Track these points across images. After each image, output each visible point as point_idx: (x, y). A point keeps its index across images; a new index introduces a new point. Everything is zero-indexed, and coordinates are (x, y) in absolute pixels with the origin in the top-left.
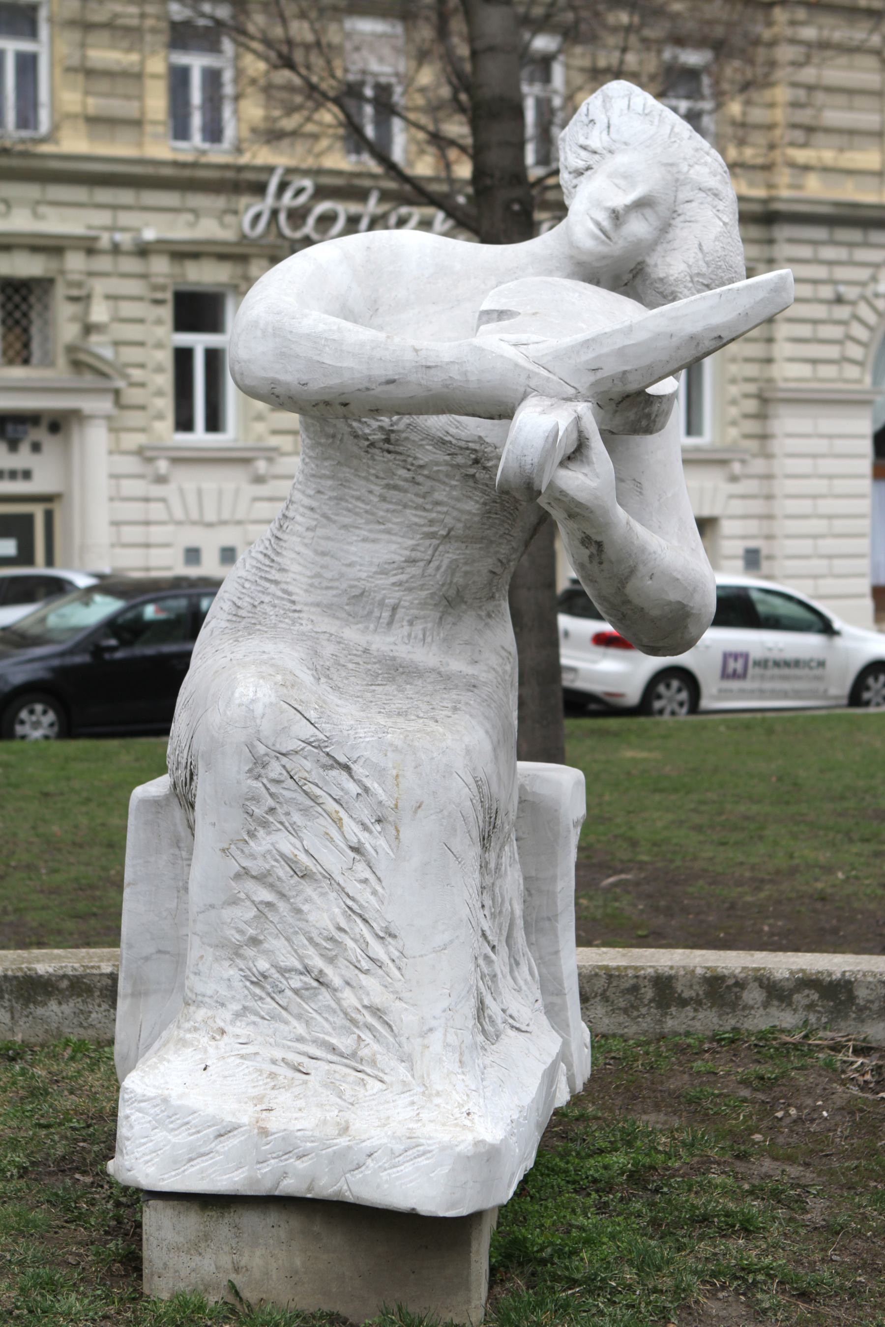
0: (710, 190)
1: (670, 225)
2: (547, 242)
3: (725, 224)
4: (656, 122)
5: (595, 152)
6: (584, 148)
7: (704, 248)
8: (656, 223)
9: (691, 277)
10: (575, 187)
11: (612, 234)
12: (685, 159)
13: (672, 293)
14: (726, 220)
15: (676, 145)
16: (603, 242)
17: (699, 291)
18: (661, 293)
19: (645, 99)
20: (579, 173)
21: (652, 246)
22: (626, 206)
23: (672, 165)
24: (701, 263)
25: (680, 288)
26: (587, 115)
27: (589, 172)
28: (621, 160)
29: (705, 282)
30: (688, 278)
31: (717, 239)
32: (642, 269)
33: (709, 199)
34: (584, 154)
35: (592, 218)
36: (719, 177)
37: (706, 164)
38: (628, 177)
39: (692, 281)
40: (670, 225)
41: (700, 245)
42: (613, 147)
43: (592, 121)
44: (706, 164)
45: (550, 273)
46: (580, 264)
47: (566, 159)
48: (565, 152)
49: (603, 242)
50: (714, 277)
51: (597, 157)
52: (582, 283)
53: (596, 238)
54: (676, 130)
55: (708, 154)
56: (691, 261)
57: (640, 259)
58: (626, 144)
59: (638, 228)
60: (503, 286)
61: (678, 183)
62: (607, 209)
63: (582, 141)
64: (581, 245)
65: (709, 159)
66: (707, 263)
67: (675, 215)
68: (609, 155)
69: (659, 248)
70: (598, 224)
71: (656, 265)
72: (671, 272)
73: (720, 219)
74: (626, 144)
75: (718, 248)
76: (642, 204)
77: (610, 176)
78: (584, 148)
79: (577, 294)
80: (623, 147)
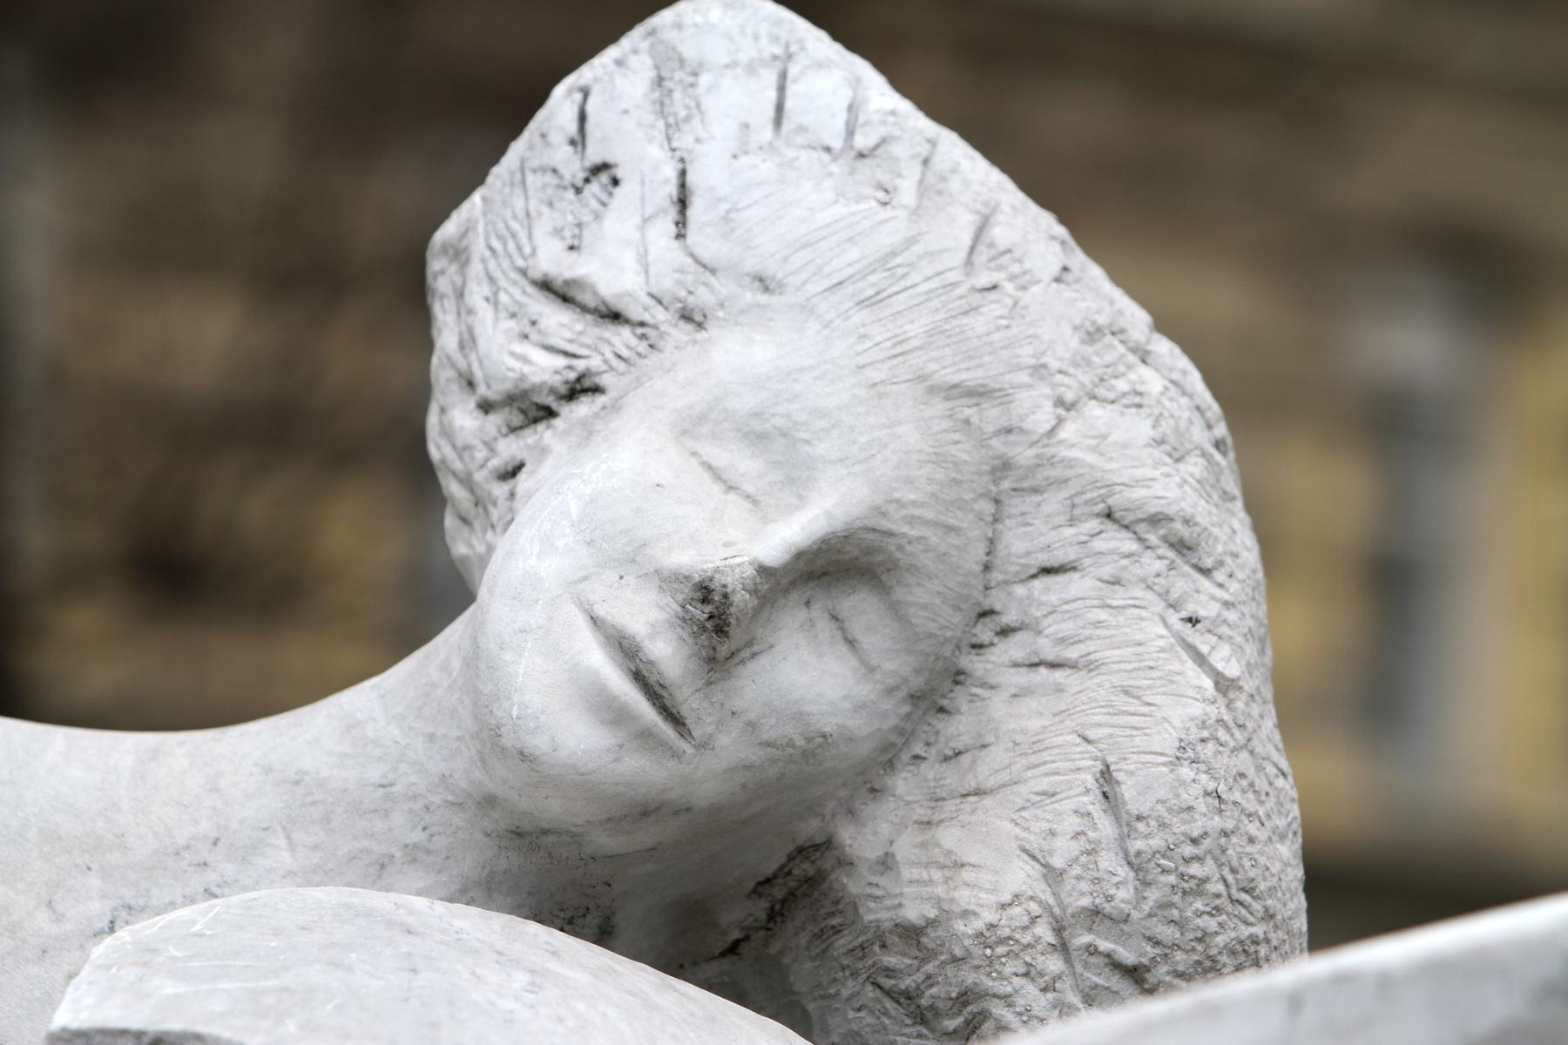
0: (1155, 520)
1: (958, 677)
2: (358, 733)
3: (1224, 685)
4: (907, 193)
5: (615, 317)
6: (560, 292)
7: (1127, 791)
8: (896, 665)
9: (1059, 930)
10: (512, 472)
11: (689, 702)
12: (1040, 370)
13: (965, 997)
14: (1232, 670)
15: (994, 308)
16: (645, 736)
17: (1092, 998)
18: (907, 997)
19: (856, 83)
20: (533, 409)
21: (873, 770)
22: (763, 571)
23: (979, 394)
24: (1109, 861)
25: (1007, 979)
26: (579, 141)
27: (583, 408)
28: (738, 357)
29: (1128, 956)
30: (1044, 932)
31: (1184, 752)
32: (815, 881)
33: (1152, 564)
34: (557, 321)
35: (594, 620)
36: (1194, 467)
37: (1136, 400)
38: (774, 439)
39: (1063, 948)
40: (958, 677)
41: (1106, 774)
42: (703, 298)
43: (601, 168)
44: (1136, 400)
45: (379, 872)
46: (524, 836)
47: (468, 342)
48: (464, 310)
49: (645, 736)
50: (1168, 933)
51: (622, 337)
52: (533, 927)
53: (613, 714)
54: (1000, 234)
55: (1144, 357)
56: (1063, 851)
57: (809, 829)
58: (763, 283)
59: (813, 678)
60: (149, 928)
61: (1006, 481)
62: (669, 580)
63: (551, 259)
64: (539, 743)
65: (1153, 382)
66: (1136, 864)
67: (984, 633)
68: (682, 333)
69: (903, 783)
70: (626, 650)
71: (886, 863)
72: (964, 897)
73: (1201, 660)
74: (763, 283)
75: (1191, 795)
76: (835, 569)
77: (689, 427)
78: (560, 292)
79: (520, 978)
80: (751, 296)
